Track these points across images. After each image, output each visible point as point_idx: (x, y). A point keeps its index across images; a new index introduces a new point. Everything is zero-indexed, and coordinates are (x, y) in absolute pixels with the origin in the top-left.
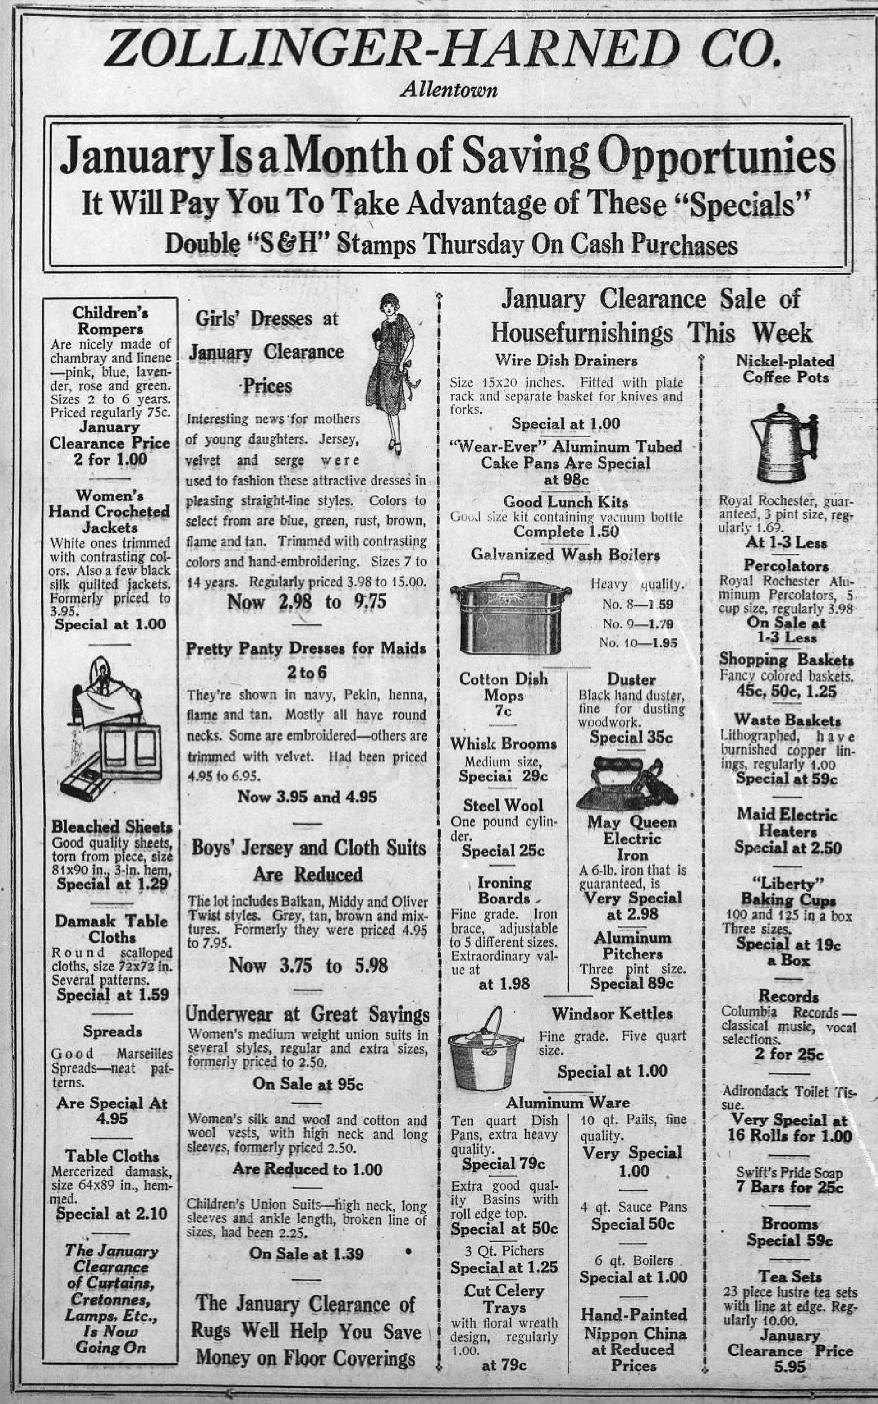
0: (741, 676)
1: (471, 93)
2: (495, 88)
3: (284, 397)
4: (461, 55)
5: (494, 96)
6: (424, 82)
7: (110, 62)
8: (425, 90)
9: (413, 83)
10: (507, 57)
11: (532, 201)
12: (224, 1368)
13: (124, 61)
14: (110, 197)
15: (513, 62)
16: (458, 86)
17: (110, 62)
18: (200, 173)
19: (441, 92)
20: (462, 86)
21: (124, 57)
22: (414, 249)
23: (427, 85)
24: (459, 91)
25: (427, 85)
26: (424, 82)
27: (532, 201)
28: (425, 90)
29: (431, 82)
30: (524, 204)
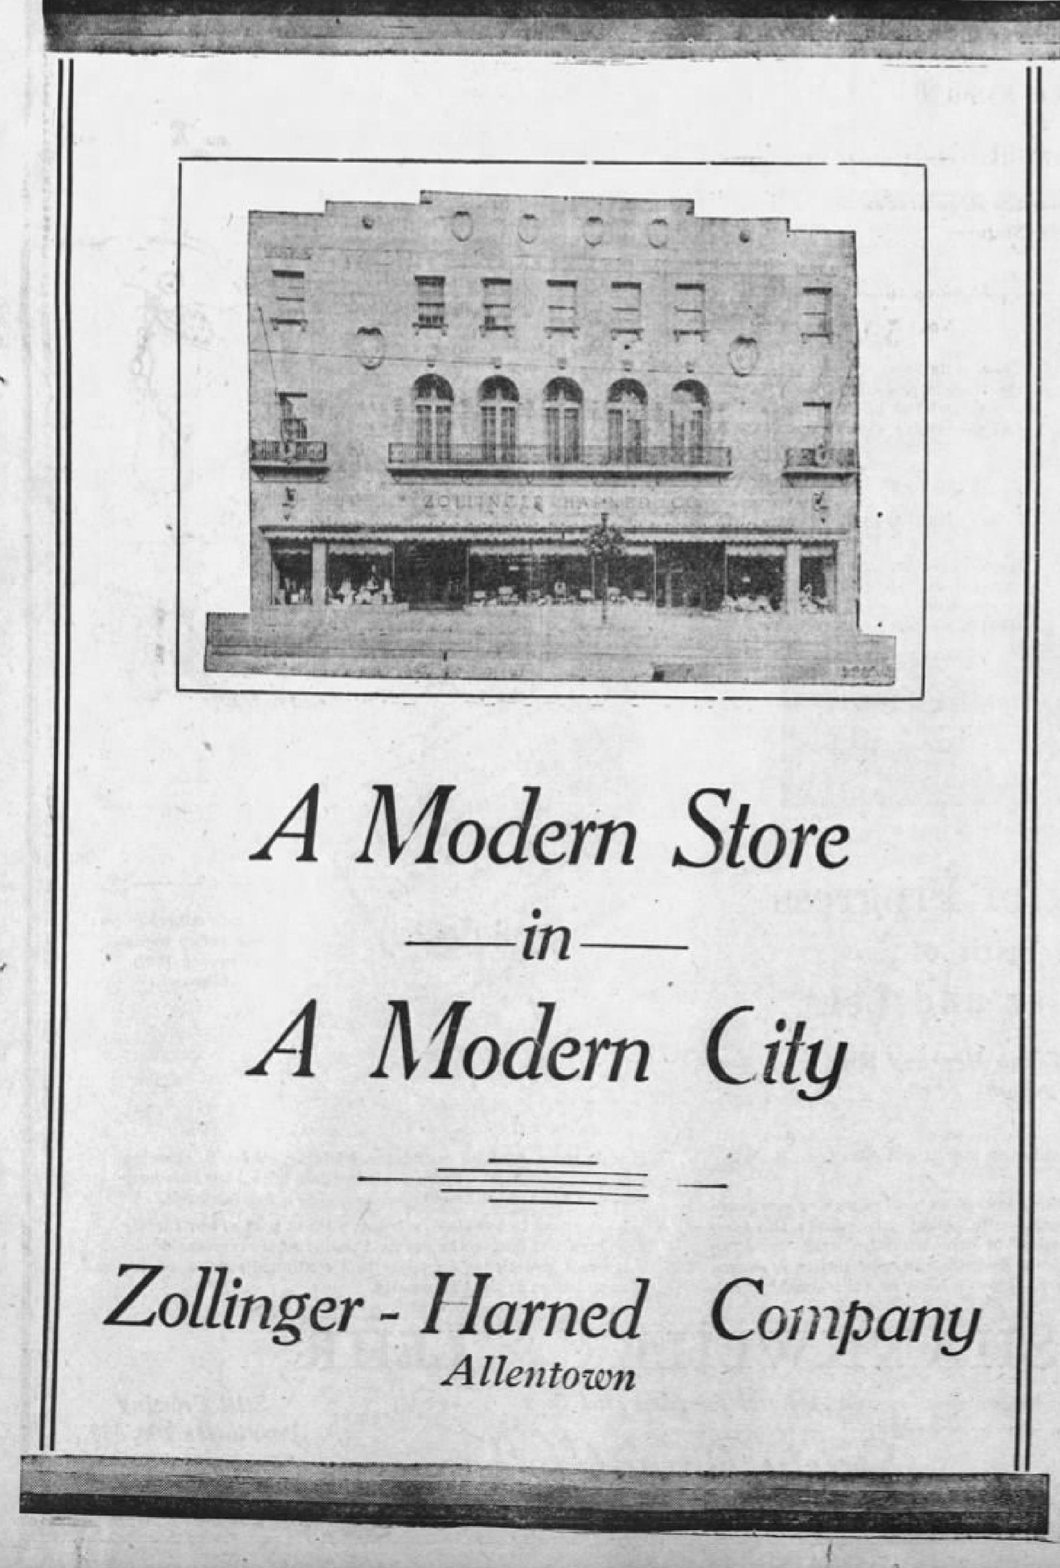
1: (582, 1381)
2: (631, 1374)
3: (807, 1334)
4: (452, 1317)
5: (629, 1387)
6: (489, 1359)
7: (112, 1320)
8: (492, 1376)
9: (468, 1359)
11: (309, 1304)
13: (498, 1311)
16: (557, 1368)
17: (112, 1320)
18: (861, 1334)
19: (524, 1377)
20: (565, 1367)
21: (138, 1310)
22: (695, 815)
23: (496, 1363)
24: (560, 1375)
25: (496, 1363)
26: (489, 1359)
27: (309, 1304)
28: (492, 1376)
29: (503, 1358)
30: (293, 1307)
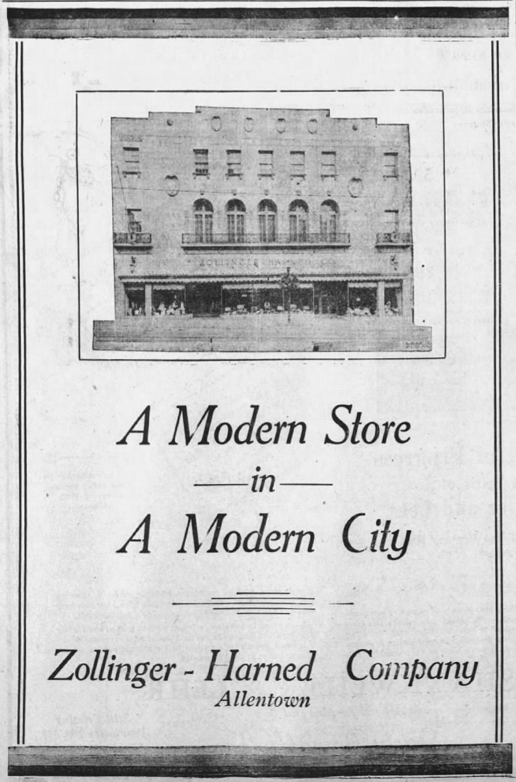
0: (108, 329)
1: (284, 703)
2: (308, 698)
5: (307, 705)
6: (238, 692)
9: (228, 693)
10: (226, 703)
11: (150, 667)
12: (370, 279)
14: (231, 704)
15: (228, 704)
19: (256, 702)
20: (275, 696)
21: (65, 673)
23: (241, 695)
24: (273, 700)
25: (241, 695)
26: (238, 692)
27: (150, 667)
28: (240, 701)
29: (245, 692)
